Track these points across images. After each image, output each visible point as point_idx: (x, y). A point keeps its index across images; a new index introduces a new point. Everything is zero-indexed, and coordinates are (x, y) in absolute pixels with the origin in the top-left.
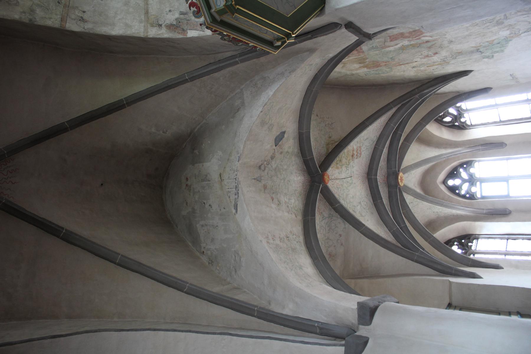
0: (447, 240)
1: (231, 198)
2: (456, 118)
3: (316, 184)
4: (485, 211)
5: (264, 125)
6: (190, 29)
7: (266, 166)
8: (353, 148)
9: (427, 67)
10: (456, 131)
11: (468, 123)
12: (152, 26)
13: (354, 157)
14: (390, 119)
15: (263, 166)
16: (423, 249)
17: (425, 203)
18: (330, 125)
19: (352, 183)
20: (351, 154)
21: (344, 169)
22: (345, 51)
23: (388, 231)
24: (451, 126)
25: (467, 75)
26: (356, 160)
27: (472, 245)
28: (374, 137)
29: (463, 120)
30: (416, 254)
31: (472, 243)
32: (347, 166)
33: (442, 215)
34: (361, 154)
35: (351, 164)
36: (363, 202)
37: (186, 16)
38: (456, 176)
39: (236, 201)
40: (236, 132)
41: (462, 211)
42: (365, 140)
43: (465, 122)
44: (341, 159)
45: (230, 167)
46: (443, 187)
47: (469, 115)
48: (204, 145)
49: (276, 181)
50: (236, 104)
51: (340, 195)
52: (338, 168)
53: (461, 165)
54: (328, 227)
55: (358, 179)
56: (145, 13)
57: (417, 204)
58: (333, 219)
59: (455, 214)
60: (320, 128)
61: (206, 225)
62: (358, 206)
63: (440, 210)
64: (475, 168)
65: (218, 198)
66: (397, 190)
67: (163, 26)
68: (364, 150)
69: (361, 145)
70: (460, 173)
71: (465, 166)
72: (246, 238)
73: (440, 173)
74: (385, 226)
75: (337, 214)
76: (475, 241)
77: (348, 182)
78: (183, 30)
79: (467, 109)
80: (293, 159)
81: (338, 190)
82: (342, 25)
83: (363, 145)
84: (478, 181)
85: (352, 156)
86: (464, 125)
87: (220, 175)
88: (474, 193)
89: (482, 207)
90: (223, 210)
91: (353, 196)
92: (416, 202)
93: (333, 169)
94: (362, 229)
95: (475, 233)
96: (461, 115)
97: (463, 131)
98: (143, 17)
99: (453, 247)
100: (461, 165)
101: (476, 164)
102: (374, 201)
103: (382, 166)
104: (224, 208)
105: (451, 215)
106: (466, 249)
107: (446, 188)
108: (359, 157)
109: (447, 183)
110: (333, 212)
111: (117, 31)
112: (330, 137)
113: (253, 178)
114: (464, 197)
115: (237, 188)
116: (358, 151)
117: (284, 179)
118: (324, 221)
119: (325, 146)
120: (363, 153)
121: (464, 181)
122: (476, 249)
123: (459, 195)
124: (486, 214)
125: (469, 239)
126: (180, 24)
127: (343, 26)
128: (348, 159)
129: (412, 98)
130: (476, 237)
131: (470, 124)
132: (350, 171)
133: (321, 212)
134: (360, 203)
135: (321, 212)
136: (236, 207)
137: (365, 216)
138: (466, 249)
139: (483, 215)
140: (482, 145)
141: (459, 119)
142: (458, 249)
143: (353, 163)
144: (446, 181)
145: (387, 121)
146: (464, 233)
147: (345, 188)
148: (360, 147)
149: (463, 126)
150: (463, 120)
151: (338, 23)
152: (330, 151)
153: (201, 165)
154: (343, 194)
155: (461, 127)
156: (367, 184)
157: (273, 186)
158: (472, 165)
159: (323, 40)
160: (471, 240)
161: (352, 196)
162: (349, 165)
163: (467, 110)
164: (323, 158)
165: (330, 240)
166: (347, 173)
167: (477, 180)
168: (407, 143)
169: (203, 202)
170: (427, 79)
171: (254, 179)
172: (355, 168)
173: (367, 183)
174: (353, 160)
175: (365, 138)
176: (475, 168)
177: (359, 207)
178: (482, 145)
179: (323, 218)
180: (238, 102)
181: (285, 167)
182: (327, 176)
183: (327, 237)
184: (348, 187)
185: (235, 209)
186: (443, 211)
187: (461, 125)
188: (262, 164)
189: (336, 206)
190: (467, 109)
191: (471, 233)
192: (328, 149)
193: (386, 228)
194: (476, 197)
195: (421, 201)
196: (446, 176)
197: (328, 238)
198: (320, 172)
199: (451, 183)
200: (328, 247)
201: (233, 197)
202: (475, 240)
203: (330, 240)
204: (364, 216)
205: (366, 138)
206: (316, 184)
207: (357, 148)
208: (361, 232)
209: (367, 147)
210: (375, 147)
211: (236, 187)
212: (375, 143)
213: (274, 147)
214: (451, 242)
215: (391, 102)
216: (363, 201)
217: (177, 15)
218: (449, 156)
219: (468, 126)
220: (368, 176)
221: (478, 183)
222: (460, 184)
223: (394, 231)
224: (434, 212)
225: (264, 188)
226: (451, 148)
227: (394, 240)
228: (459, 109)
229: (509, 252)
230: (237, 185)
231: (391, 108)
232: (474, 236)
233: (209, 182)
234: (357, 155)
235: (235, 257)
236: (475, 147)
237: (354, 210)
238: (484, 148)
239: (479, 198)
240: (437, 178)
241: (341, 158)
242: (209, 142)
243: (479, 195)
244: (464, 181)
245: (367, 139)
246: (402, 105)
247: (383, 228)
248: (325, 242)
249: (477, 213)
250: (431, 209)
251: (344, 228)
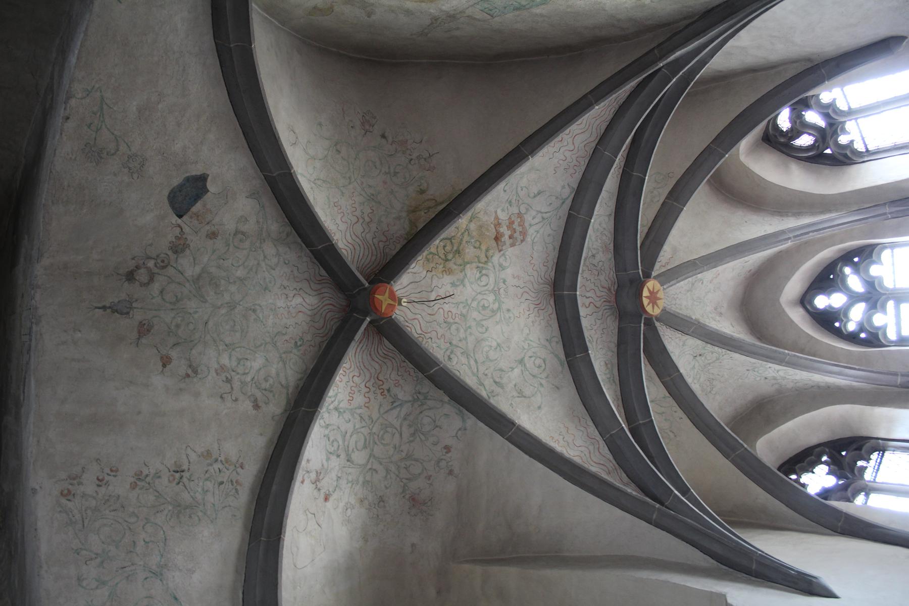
0: (804, 448)
2: (826, 135)
3: (355, 314)
4: (899, 380)
5: (101, 158)
7: (156, 270)
8: (497, 218)
10: (826, 170)
11: (859, 146)
13: (505, 243)
15: (142, 271)
16: (685, 491)
17: (736, 356)
18: (425, 159)
19: (499, 308)
20: (493, 233)
21: (471, 272)
23: (599, 438)
26: (510, 249)
27: (866, 467)
28: (563, 187)
29: (843, 140)
30: (654, 507)
31: (868, 463)
32: (481, 265)
33: (790, 386)
34: (524, 234)
35: (495, 259)
36: (533, 359)
38: (833, 286)
41: (838, 376)
42: (535, 197)
44: (458, 247)
46: (797, 316)
47: (858, 124)
49: (196, 312)
51: (454, 342)
52: (449, 272)
53: (847, 258)
54: (410, 426)
55: (523, 300)
57: (718, 359)
58: (425, 407)
59: (822, 384)
60: (389, 168)
62: (513, 369)
63: (780, 373)
64: (882, 264)
66: (640, 326)
68: (534, 222)
69: (523, 210)
70: (843, 278)
71: (856, 259)
73: (788, 279)
74: (591, 423)
75: (442, 392)
76: (875, 456)
77: (484, 307)
79: (850, 108)
80: (269, 249)
81: (450, 329)
83: (527, 210)
84: (888, 299)
85: (497, 239)
86: (846, 154)
88: (879, 328)
89: (893, 369)
91: (498, 345)
92: (712, 353)
93: (433, 273)
94: (510, 434)
95: (875, 436)
96: (835, 127)
97: (845, 167)
99: (816, 468)
100: (847, 258)
101: (886, 255)
102: (567, 355)
103: (601, 263)
105: (812, 387)
106: (847, 476)
107: (807, 316)
108: (519, 240)
109: (811, 303)
110: (427, 387)
112: (422, 192)
113: (100, 305)
114: (852, 338)
116: (515, 226)
117: (232, 306)
118: (395, 412)
119: (404, 214)
120: (531, 231)
121: (855, 298)
122: (877, 480)
123: (839, 334)
124: (902, 386)
125: (859, 449)
128: (484, 248)
130: (879, 444)
131: (864, 150)
132: (492, 280)
133: (385, 387)
134: (521, 361)
135: (385, 387)
137: (533, 396)
138: (847, 478)
139: (896, 389)
140: (893, 202)
141: (831, 137)
142: (828, 474)
143: (503, 258)
144: (808, 297)
145: (594, 145)
146: (848, 434)
147: (473, 324)
148: (520, 215)
149: (846, 156)
150: (843, 140)
152: (421, 226)
154: (466, 339)
155: (841, 158)
156: (549, 312)
157: (178, 326)
160: (863, 452)
161: (494, 344)
162: (490, 264)
163: (851, 113)
164: (399, 247)
165: (416, 460)
166: (483, 283)
167: (885, 294)
168: (675, 203)
170: (685, 18)
171: (104, 308)
172: (509, 271)
173: (551, 309)
174: (500, 251)
175: (535, 190)
176: (882, 264)
177: (517, 371)
178: (893, 202)
179: (393, 403)
181: (240, 273)
182: (387, 294)
183: (404, 454)
184: (485, 320)
186: (787, 377)
188: (138, 267)
189: (432, 372)
190: (850, 108)
191: (865, 433)
192: (413, 224)
193: (592, 429)
194: (883, 341)
195: (724, 350)
196: (807, 285)
197: (409, 457)
198: (363, 285)
199: (821, 302)
200: (407, 479)
202: (878, 452)
203: (416, 460)
204: (529, 397)
205: (536, 192)
206: (355, 314)
207: (510, 218)
208: (510, 440)
209: (545, 216)
210: (570, 216)
212: (569, 202)
213: (174, 219)
214: (812, 455)
216: (531, 357)
218: (802, 234)
219: (860, 154)
220: (554, 291)
221: (890, 305)
222: (844, 304)
223: (611, 436)
224: (766, 378)
225: (139, 332)
226: (813, 214)
227: (610, 461)
228: (829, 111)
229: (891, 532)
232: (873, 441)
234: (510, 237)
236: (872, 209)
237: (497, 380)
238: (897, 211)
239: (892, 342)
240: (781, 291)
241: (460, 244)
243: (892, 335)
244: (855, 298)
245: (539, 193)
247: (582, 429)
248: (399, 467)
249: (884, 383)
250: (756, 370)
251: (460, 429)
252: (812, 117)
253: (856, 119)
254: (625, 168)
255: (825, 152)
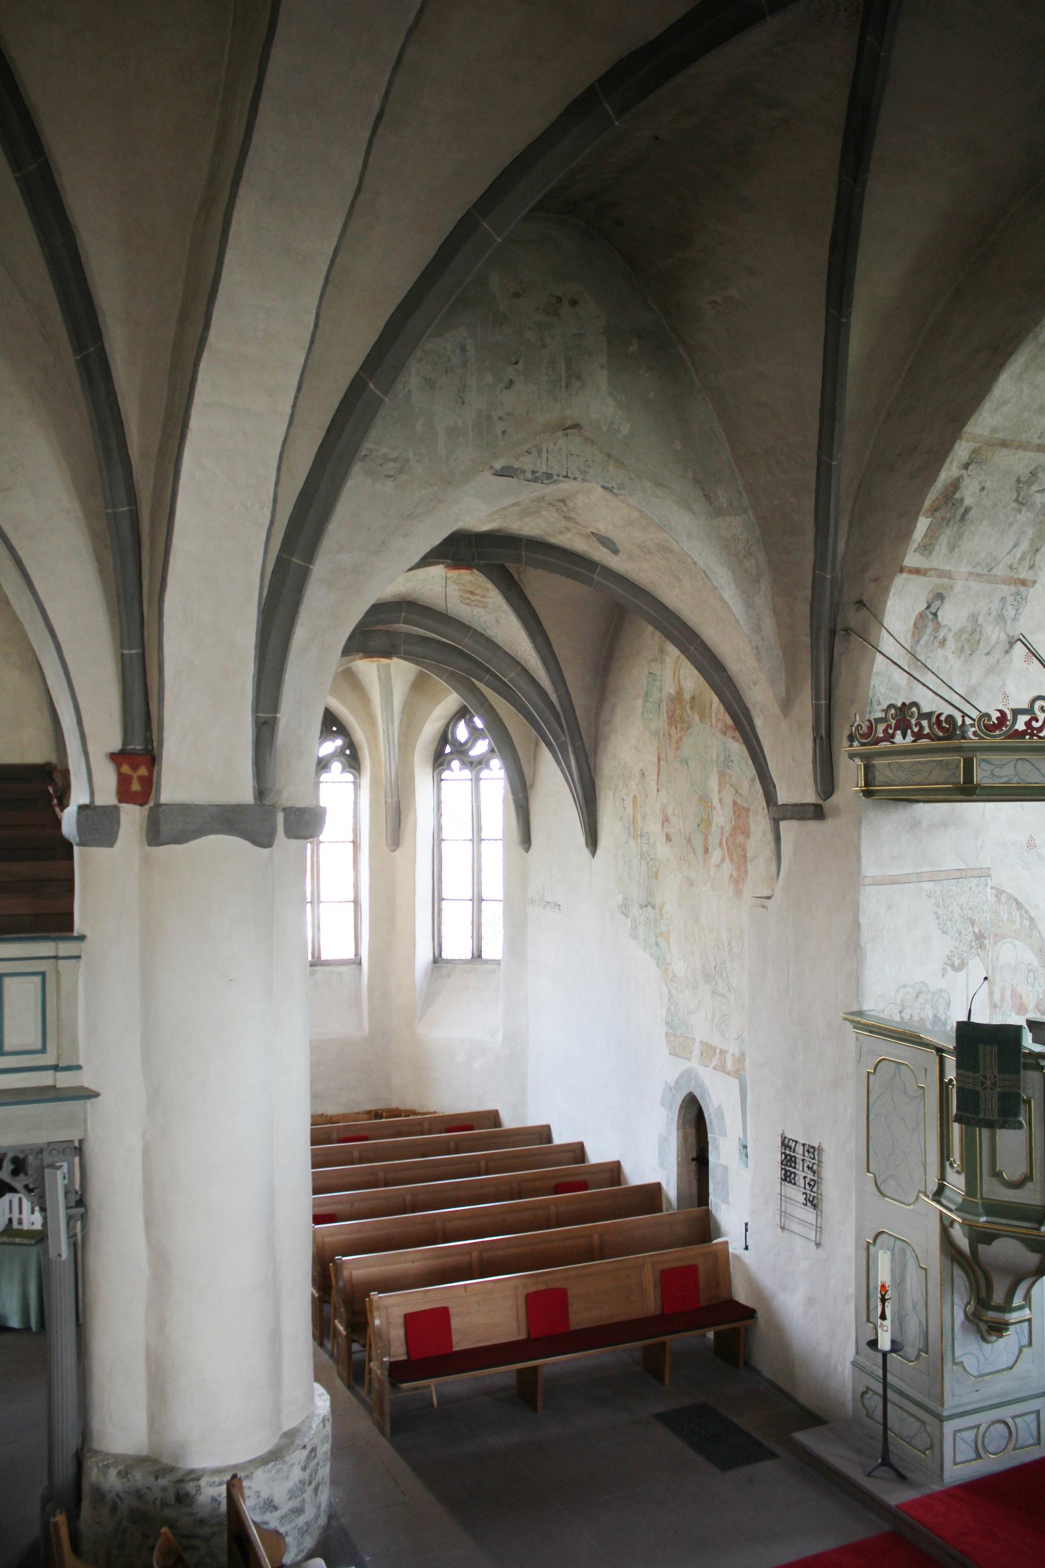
1: (527, 459)
2: (461, 751)
6: (931, 522)
9: (635, 797)
10: (433, 747)
11: (446, 775)
12: (975, 451)
14: (525, 672)
22: (758, 750)
24: (445, 738)
25: (587, 845)
29: (455, 764)
37: (959, 517)
39: (519, 472)
40: (665, 486)
42: (496, 619)
43: (449, 768)
45: (592, 461)
48: (647, 375)
50: (720, 493)
56: (1004, 441)
61: (465, 363)
65: (528, 412)
67: (964, 472)
71: (348, 752)
72: (440, 501)
78: (936, 510)
79: (481, 779)
82: (825, 800)
85: (472, 593)
86: (443, 765)
87: (577, 426)
90: (499, 427)
98: (1000, 435)
104: (504, 432)
111: (1005, 385)
115: (548, 479)
120: (468, 609)
126: (951, 505)
127: (820, 802)
129: (567, 733)
131: (442, 777)
136: (507, 474)
149: (441, 764)
150: (455, 764)
151: (829, 797)
153: (603, 359)
158: (348, 769)
159: (805, 748)
169: (520, 358)
178: (399, 802)
180: (722, 497)
185: (503, 468)
187: (444, 761)
190: (481, 779)
201: (527, 463)
210: (469, 628)
211: (549, 476)
215: (567, 690)
217: (968, 501)
219: (440, 774)
230: (552, 480)
231: (556, 690)
233: (564, 384)
235: (395, 460)
242: (651, 395)
246: (559, 714)
252: (481, 747)
253: (472, 840)
254: (473, 210)
255: (448, 746)
